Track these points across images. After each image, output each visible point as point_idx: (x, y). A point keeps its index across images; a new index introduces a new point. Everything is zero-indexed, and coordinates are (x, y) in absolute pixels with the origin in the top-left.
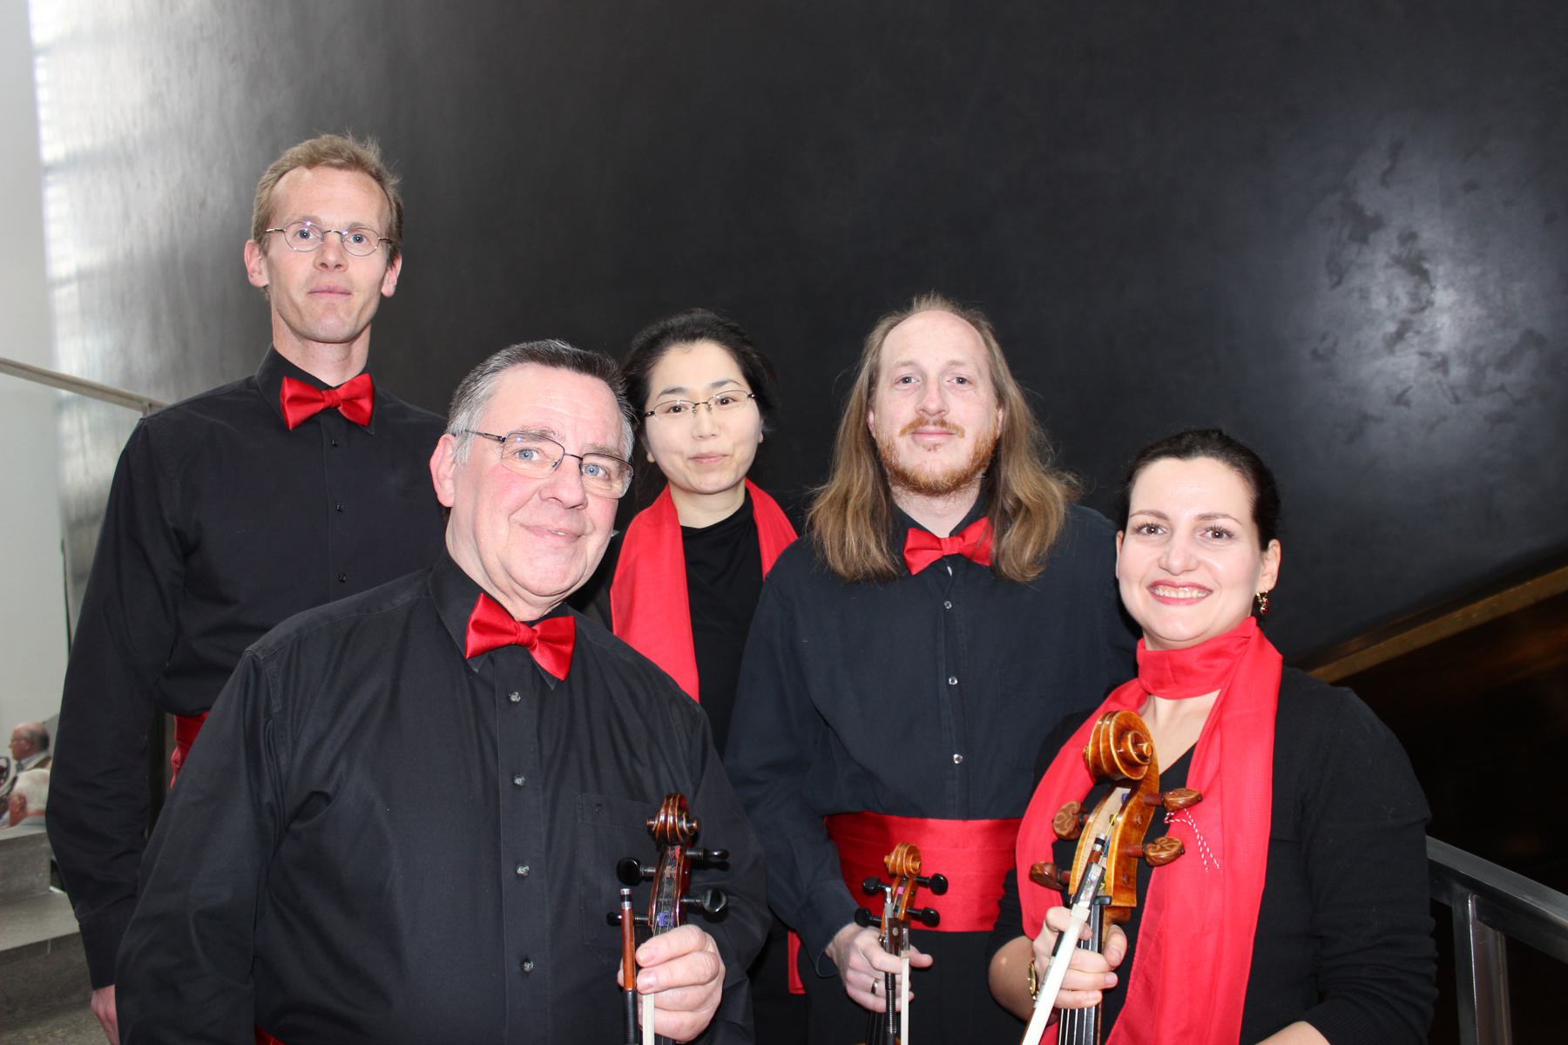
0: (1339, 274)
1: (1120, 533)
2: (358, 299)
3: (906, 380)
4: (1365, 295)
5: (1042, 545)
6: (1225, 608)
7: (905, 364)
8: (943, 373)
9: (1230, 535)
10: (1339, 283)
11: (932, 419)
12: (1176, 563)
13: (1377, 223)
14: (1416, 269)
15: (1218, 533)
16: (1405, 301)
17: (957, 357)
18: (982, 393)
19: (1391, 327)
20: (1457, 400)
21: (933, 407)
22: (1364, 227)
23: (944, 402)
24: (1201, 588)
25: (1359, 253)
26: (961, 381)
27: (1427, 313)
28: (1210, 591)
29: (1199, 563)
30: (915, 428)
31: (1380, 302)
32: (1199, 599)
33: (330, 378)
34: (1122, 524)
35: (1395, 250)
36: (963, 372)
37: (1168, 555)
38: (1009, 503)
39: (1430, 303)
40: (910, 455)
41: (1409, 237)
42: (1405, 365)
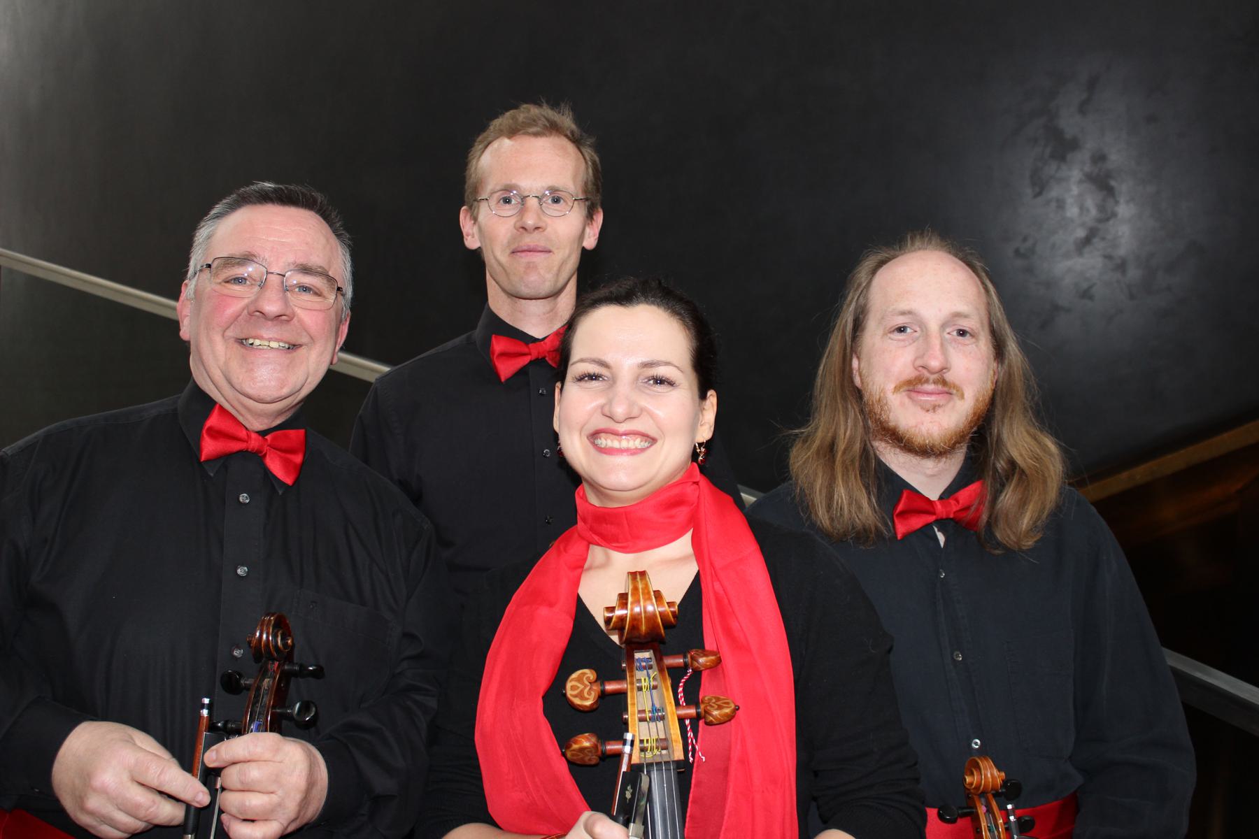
0: (1040, 186)
1: (559, 384)
2: (558, 257)
3: (901, 330)
4: (1061, 204)
5: (1042, 511)
6: (670, 456)
7: (903, 313)
8: (943, 326)
9: (671, 384)
10: (1040, 194)
11: (932, 377)
12: (620, 410)
13: (1074, 145)
14: (1102, 183)
15: (659, 381)
16: (1094, 212)
17: (962, 308)
18: (982, 346)
19: (1081, 233)
20: (1132, 297)
21: (935, 364)
22: (1063, 148)
23: (947, 360)
24: (644, 436)
25: (1059, 168)
26: (962, 333)
27: (1111, 222)
28: (653, 440)
29: (642, 410)
30: (912, 386)
31: (1072, 211)
32: (643, 450)
33: (207, 754)
34: (561, 376)
35: (1087, 168)
36: (965, 324)
37: (610, 402)
38: (1001, 465)
39: (1114, 215)
40: (907, 415)
41: (1099, 158)
42: (1090, 264)
